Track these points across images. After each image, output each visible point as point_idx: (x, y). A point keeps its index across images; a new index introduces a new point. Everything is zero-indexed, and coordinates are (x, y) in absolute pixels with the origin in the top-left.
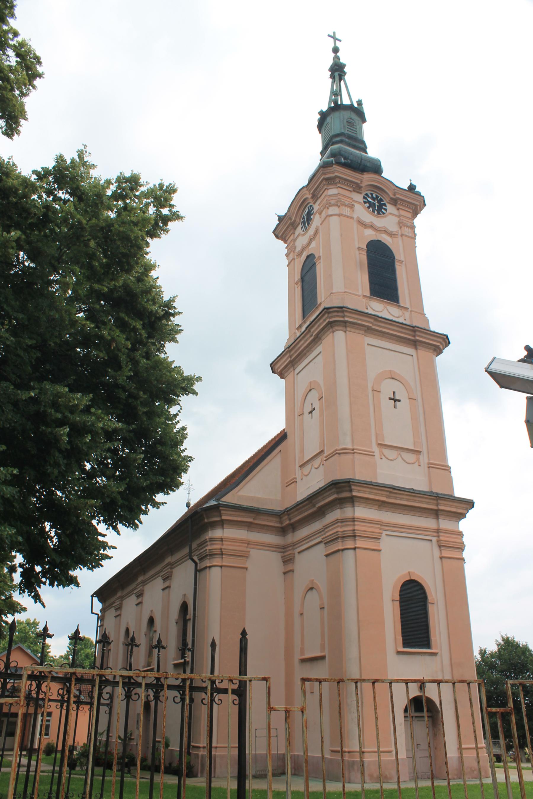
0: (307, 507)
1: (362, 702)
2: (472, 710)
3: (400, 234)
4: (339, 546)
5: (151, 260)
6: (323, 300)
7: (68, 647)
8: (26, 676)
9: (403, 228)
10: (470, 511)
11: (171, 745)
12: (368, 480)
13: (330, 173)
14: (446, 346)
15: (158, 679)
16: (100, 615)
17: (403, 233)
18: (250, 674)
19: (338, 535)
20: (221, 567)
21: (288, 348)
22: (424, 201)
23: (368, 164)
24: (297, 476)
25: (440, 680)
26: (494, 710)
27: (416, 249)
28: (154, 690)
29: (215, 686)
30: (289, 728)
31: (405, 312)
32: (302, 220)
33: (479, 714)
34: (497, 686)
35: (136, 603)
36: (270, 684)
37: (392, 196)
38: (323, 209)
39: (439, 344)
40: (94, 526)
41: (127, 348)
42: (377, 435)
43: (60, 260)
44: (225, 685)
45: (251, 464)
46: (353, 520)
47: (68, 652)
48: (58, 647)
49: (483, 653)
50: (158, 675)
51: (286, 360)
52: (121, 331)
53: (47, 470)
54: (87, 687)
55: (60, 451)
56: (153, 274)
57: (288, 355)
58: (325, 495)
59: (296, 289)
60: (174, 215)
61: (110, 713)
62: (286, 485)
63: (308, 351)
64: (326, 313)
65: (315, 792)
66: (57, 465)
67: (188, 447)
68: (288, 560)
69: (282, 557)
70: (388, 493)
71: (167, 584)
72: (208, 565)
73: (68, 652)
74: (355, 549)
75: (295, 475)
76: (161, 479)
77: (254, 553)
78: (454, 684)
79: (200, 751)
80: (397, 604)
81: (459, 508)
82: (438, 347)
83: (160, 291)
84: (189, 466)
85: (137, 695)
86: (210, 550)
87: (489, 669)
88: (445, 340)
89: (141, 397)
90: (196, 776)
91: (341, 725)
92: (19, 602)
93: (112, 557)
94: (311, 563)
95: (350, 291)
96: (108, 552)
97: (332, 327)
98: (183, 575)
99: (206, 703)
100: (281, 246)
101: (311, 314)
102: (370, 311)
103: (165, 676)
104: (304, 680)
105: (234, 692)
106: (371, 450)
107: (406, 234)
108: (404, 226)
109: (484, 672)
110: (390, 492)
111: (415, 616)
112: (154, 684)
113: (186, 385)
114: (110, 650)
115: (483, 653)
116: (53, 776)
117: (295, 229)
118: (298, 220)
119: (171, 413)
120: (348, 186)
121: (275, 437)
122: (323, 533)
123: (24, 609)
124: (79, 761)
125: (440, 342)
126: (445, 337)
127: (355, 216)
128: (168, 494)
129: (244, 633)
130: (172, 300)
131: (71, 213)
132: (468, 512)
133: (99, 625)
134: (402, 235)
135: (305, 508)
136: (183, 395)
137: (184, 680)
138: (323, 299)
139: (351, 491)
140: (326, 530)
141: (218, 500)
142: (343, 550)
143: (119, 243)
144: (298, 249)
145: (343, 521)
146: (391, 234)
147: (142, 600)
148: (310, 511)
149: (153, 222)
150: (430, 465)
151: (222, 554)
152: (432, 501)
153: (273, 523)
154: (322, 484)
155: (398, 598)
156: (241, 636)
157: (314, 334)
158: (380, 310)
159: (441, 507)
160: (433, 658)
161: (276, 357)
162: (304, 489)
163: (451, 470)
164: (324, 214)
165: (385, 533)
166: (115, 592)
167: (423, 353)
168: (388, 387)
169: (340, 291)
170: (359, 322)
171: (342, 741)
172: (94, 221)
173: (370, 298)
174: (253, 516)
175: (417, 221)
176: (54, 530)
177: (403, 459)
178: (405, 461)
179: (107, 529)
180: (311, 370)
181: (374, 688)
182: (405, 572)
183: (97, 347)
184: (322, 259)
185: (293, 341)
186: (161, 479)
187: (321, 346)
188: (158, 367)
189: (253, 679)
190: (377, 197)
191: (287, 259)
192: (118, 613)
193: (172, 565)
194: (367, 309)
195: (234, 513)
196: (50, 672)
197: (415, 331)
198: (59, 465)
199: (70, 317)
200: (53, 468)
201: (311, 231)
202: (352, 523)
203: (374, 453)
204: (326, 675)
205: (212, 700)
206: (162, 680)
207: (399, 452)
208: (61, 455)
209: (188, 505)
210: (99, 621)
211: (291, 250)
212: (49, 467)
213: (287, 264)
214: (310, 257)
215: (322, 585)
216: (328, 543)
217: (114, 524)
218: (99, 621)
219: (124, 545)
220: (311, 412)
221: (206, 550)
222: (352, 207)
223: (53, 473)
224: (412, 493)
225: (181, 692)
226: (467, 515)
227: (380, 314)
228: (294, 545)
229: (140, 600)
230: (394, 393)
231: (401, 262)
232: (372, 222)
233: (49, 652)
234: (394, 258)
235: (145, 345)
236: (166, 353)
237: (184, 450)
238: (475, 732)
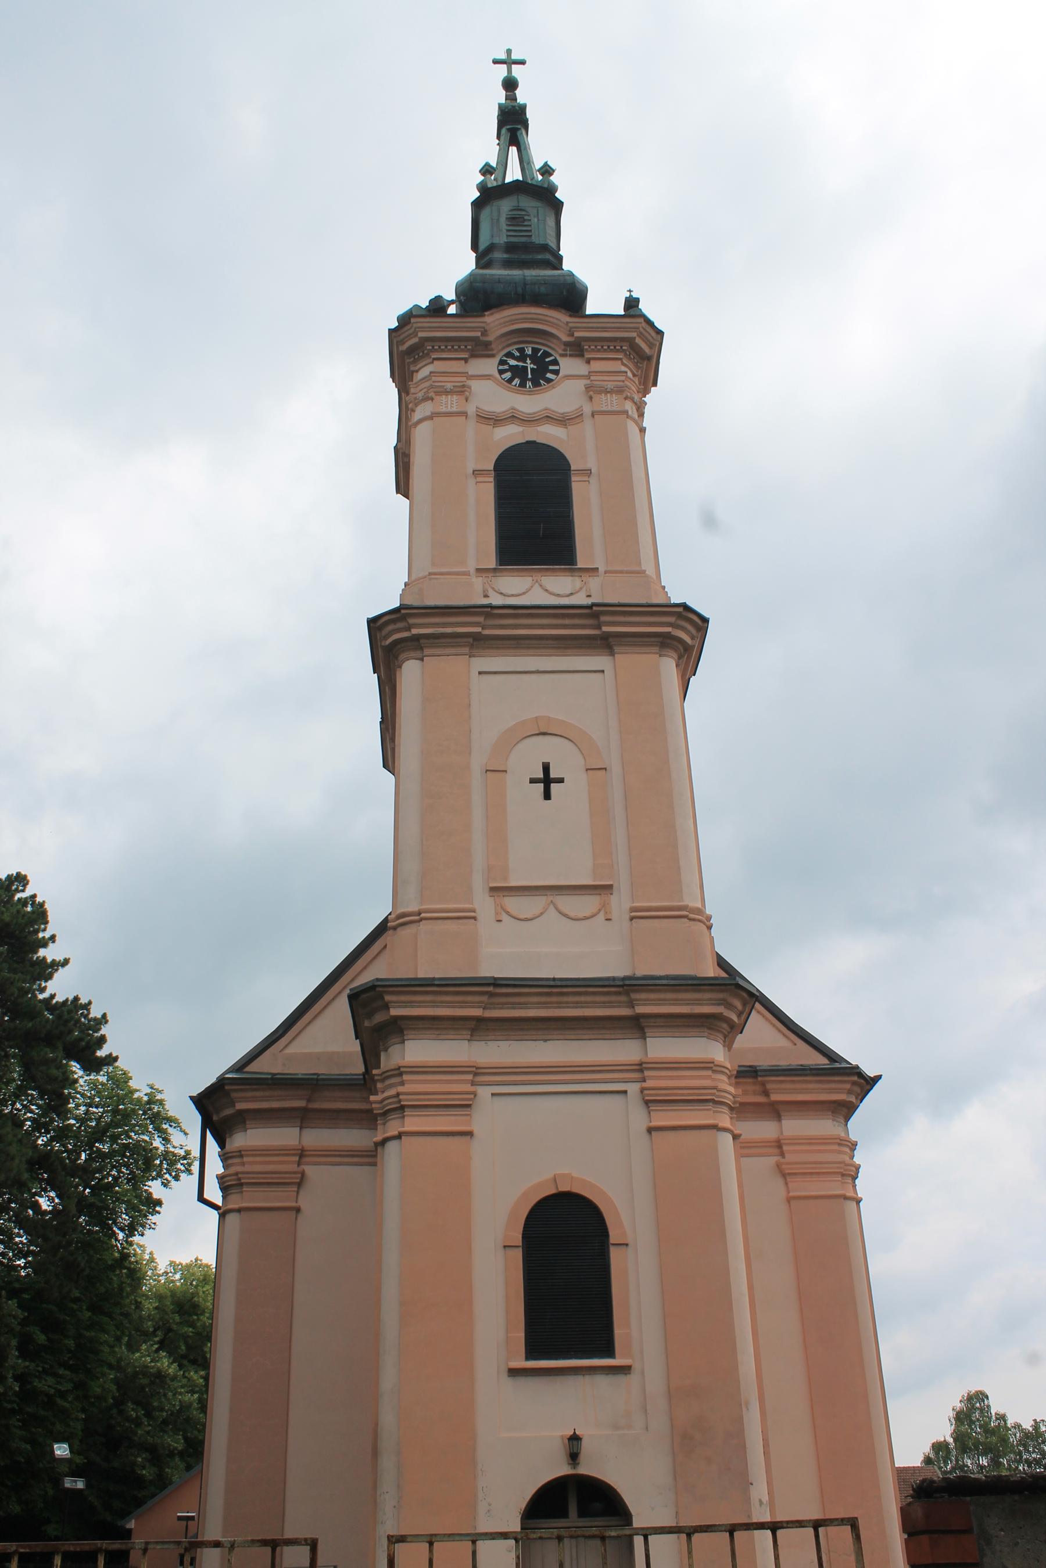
9: (596, 398)
13: (409, 337)
22: (650, 323)
23: (543, 290)
37: (565, 338)
39: (669, 629)
70: (485, 998)
80: (518, 1254)
102: (496, 600)
106: (467, 906)
108: (600, 392)
110: (491, 995)
120: (456, 350)
125: (670, 625)
152: (614, 998)
159: (640, 1010)
160: (621, 1379)
165: (484, 1092)
170: (449, 630)
190: (521, 350)
194: (486, 596)
197: (596, 616)
207: (550, 898)
222: (462, 391)
231: (588, 472)
232: (513, 409)
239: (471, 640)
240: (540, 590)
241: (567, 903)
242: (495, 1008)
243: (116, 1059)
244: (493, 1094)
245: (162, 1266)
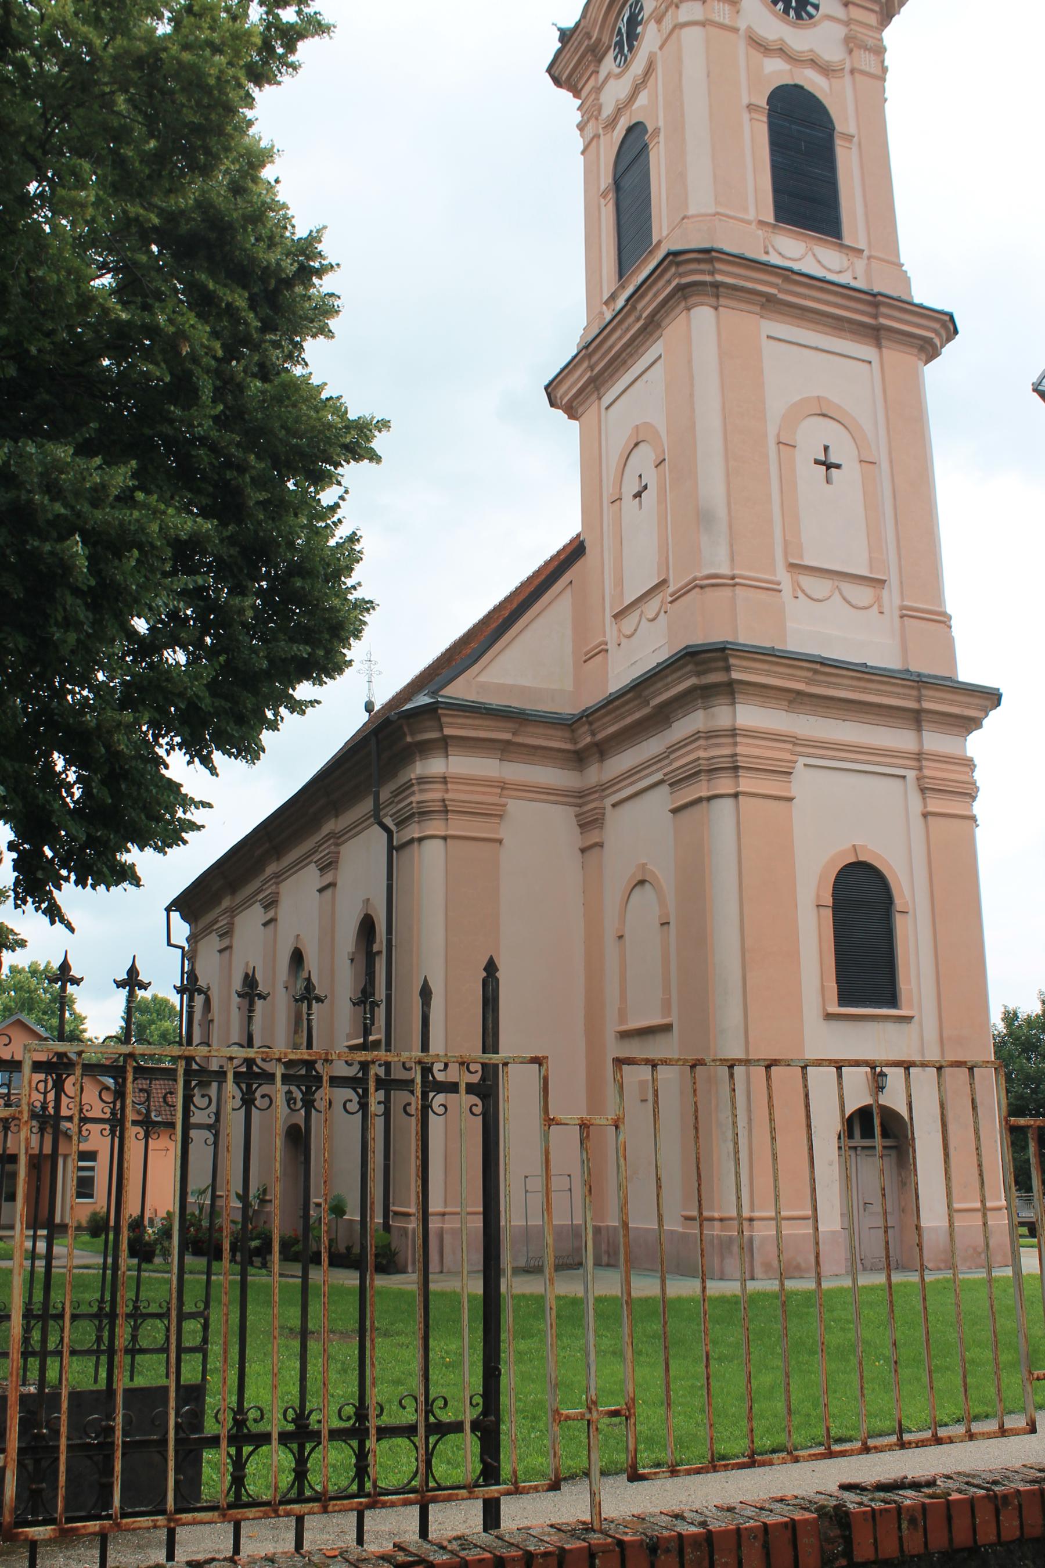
0: (631, 705)
1: (750, 1120)
2: (976, 1123)
3: (848, 67)
4: (701, 789)
5: (260, 139)
6: (665, 233)
8: (30, 1063)
9: (856, 52)
10: (992, 713)
11: (347, 1210)
12: (767, 644)
14: (949, 339)
15: (310, 1064)
16: (187, 948)
17: (856, 66)
18: (505, 1052)
19: (699, 765)
20: (445, 838)
21: (586, 347)
24: (608, 638)
25: (909, 1061)
26: (1022, 1121)
27: (887, 105)
28: (303, 1088)
29: (431, 1078)
30: (588, 1160)
31: (855, 260)
32: (615, 39)
33: (996, 1141)
34: (1038, 1087)
36: (547, 1070)
38: (667, 10)
40: (161, 757)
41: (215, 358)
42: (786, 544)
43: (47, 147)
44: (453, 1075)
45: (506, 613)
46: (733, 733)
48: (100, 1016)
49: (1010, 1018)
50: (310, 1054)
51: (580, 377)
52: (199, 316)
53: (53, 635)
54: (158, 1087)
55: (76, 591)
56: (268, 173)
57: (585, 364)
58: (669, 679)
59: (603, 209)
60: (309, 22)
61: (216, 1144)
62: (585, 658)
63: (631, 355)
64: (671, 263)
65: (650, 1298)
66: (69, 623)
67: (364, 581)
68: (590, 822)
69: (576, 816)
70: (809, 674)
71: (328, 878)
72: (416, 835)
74: (736, 795)
76: (304, 651)
77: (515, 807)
78: (939, 1069)
79: (409, 1222)
80: (829, 913)
81: (968, 706)
82: (928, 341)
83: (285, 218)
84: (365, 623)
85: (267, 1099)
86: (418, 802)
87: (1024, 1051)
88: (947, 326)
89: (254, 467)
90: (403, 1271)
91: (698, 1153)
92: (10, 927)
93: (203, 827)
94: (641, 828)
95: (732, 213)
96: (196, 815)
97: (685, 298)
98: (363, 857)
99: (413, 1112)
100: (566, 104)
101: (638, 267)
102: (775, 259)
103: (323, 1056)
104: (619, 1062)
105: (471, 1089)
106: (773, 578)
107: (863, 68)
108: (860, 47)
109: (1011, 1056)
110: (816, 672)
111: (862, 935)
112: (302, 1076)
113: (355, 441)
114: (212, 1021)
115: (1010, 1018)
116: (104, 1274)
117: (600, 61)
118: (605, 39)
119: (324, 503)
121: (559, 553)
122: (666, 762)
123: (22, 944)
124: (159, 1247)
125: (935, 331)
126: (947, 318)
127: (742, 26)
128: (321, 683)
129: (491, 967)
130: (314, 238)
131: (65, 23)
132: (987, 715)
134: (852, 72)
135: (627, 707)
136: (348, 462)
137: (364, 1066)
138: (667, 232)
139: (728, 669)
140: (672, 757)
141: (434, 693)
142: (710, 799)
143: (181, 99)
144: (608, 111)
145: (711, 735)
146: (826, 70)
147: (276, 913)
148: (637, 716)
149: (258, 41)
150: (905, 612)
151: (447, 812)
153: (557, 741)
154: (663, 656)
155: (829, 901)
156: (485, 974)
157: (644, 315)
158: (797, 256)
159: (926, 705)
160: (904, 1027)
161: (558, 370)
162: (623, 669)
163: (953, 622)
164: (668, 22)
165: (802, 761)
166: (215, 900)
167: (896, 356)
168: (814, 434)
169: (703, 211)
171: (699, 1185)
172: (119, 40)
173: (774, 226)
174: (512, 727)
175: (891, 35)
176: (74, 769)
177: (844, 599)
178: (849, 602)
179: (189, 763)
180: (639, 398)
181: (768, 1077)
182: (847, 845)
183: (148, 354)
184: (662, 135)
185: (597, 331)
186: (304, 651)
187: (660, 342)
188: (289, 398)
189: (511, 1061)
191: (582, 136)
192: (225, 943)
193: (338, 838)
194: (767, 253)
195: (469, 721)
196: (79, 1054)
197: (876, 305)
198: (78, 625)
199: (79, 287)
200: (66, 632)
201: (638, 66)
202: (729, 740)
203: (779, 584)
204: (672, 1053)
205: (426, 1108)
206: (319, 1066)
207: (836, 583)
208: (79, 601)
209: (369, 707)
210: (186, 962)
211: (590, 113)
212: (55, 629)
213: (581, 148)
214: (636, 130)
215: (664, 873)
216: (675, 784)
217: (205, 752)
218: (186, 962)
219: (229, 798)
220: (638, 495)
223: (65, 642)
224: (863, 672)
225: (360, 1091)
226: (985, 722)
227: (796, 266)
228: (603, 789)
229: (271, 914)
230: (826, 449)
231: (849, 138)
232: (781, 40)
233: (84, 1031)
234: (833, 129)
235: (256, 347)
236: (307, 364)
237: (354, 588)
238: (980, 1166)
239: (764, 300)
240: (813, 260)
241: (852, 591)
242: (813, 685)
244: (805, 765)
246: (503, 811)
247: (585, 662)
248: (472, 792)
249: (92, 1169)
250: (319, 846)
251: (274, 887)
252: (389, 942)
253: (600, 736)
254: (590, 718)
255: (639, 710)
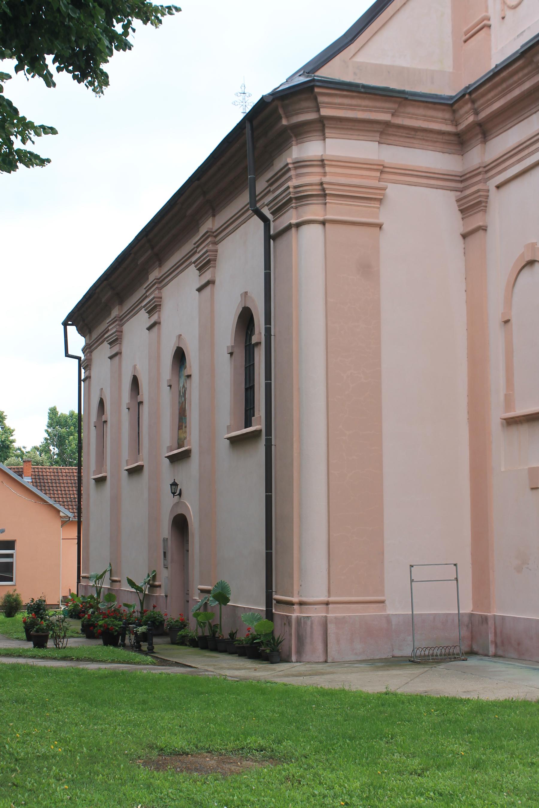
0: (520, 74)
7: (47, 431)
11: (231, 597)
16: (83, 358)
20: (323, 223)
35: (148, 325)
47: (46, 439)
62: (464, 38)
68: (472, 206)
69: (458, 201)
72: (294, 221)
73: (46, 439)
75: (487, 11)
77: (395, 192)
79: (293, 611)
86: (295, 187)
90: (287, 660)
93: (49, 161)
96: (38, 145)
98: (240, 253)
114: (105, 422)
133: (83, 377)
135: (515, 78)
147: (159, 317)
151: (325, 195)
153: (438, 123)
166: (106, 310)
174: (390, 108)
221: (288, 188)
228: (487, 170)
229: (155, 318)
233: (13, 441)
243: (161, 23)
245: (59, 414)
246: (384, 195)
247: (465, 41)
248: (351, 176)
249: (11, 556)
250: (198, 247)
251: (157, 292)
252: (268, 331)
253: (483, 115)
254: (473, 96)
255: (529, 79)
